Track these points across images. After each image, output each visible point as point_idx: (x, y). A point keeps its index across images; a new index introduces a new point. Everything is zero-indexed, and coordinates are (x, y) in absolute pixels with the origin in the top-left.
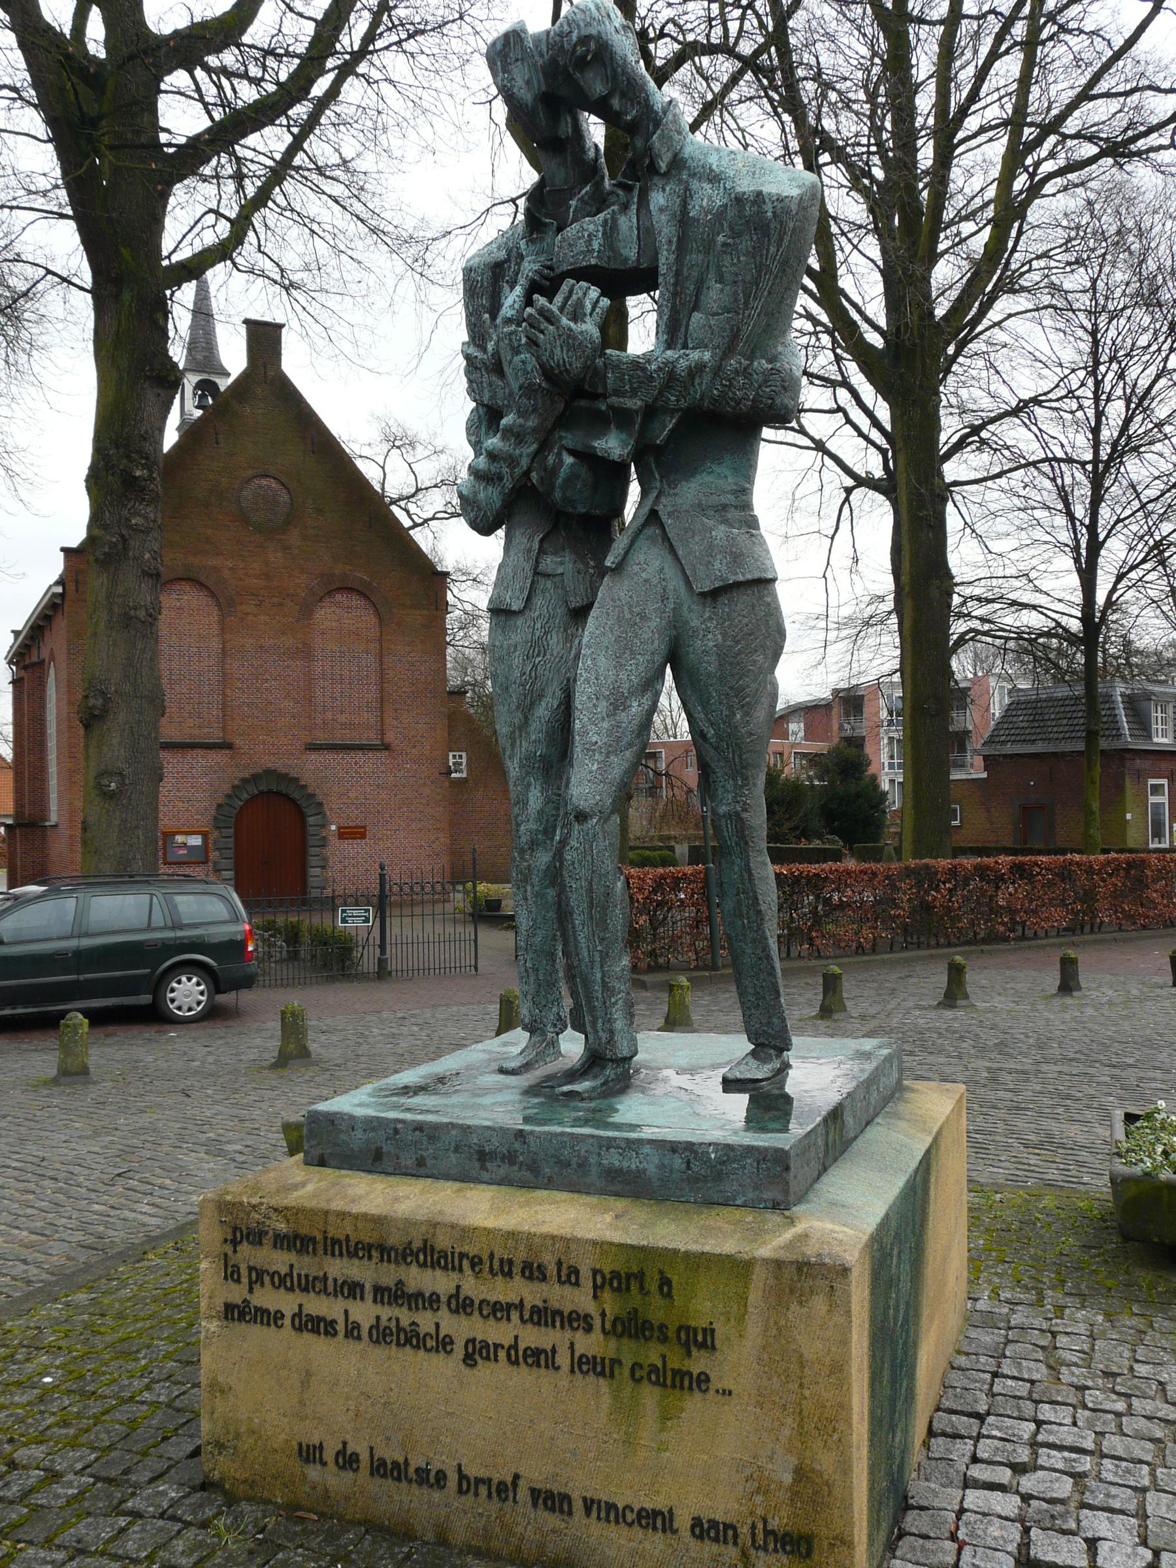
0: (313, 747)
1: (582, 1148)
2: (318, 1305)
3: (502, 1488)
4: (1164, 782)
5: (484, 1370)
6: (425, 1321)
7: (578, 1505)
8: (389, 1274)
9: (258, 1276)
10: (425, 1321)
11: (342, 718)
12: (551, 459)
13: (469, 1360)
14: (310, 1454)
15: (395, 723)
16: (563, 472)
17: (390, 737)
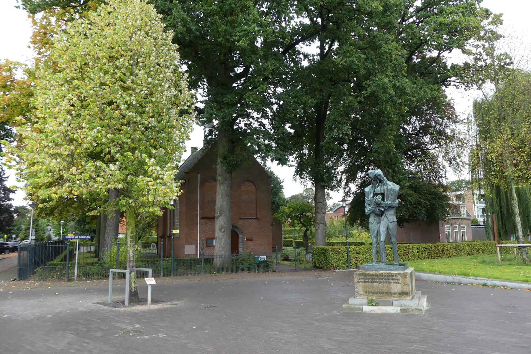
0: (240, 219)
8: (372, 277)
11: (247, 212)
17: (258, 216)
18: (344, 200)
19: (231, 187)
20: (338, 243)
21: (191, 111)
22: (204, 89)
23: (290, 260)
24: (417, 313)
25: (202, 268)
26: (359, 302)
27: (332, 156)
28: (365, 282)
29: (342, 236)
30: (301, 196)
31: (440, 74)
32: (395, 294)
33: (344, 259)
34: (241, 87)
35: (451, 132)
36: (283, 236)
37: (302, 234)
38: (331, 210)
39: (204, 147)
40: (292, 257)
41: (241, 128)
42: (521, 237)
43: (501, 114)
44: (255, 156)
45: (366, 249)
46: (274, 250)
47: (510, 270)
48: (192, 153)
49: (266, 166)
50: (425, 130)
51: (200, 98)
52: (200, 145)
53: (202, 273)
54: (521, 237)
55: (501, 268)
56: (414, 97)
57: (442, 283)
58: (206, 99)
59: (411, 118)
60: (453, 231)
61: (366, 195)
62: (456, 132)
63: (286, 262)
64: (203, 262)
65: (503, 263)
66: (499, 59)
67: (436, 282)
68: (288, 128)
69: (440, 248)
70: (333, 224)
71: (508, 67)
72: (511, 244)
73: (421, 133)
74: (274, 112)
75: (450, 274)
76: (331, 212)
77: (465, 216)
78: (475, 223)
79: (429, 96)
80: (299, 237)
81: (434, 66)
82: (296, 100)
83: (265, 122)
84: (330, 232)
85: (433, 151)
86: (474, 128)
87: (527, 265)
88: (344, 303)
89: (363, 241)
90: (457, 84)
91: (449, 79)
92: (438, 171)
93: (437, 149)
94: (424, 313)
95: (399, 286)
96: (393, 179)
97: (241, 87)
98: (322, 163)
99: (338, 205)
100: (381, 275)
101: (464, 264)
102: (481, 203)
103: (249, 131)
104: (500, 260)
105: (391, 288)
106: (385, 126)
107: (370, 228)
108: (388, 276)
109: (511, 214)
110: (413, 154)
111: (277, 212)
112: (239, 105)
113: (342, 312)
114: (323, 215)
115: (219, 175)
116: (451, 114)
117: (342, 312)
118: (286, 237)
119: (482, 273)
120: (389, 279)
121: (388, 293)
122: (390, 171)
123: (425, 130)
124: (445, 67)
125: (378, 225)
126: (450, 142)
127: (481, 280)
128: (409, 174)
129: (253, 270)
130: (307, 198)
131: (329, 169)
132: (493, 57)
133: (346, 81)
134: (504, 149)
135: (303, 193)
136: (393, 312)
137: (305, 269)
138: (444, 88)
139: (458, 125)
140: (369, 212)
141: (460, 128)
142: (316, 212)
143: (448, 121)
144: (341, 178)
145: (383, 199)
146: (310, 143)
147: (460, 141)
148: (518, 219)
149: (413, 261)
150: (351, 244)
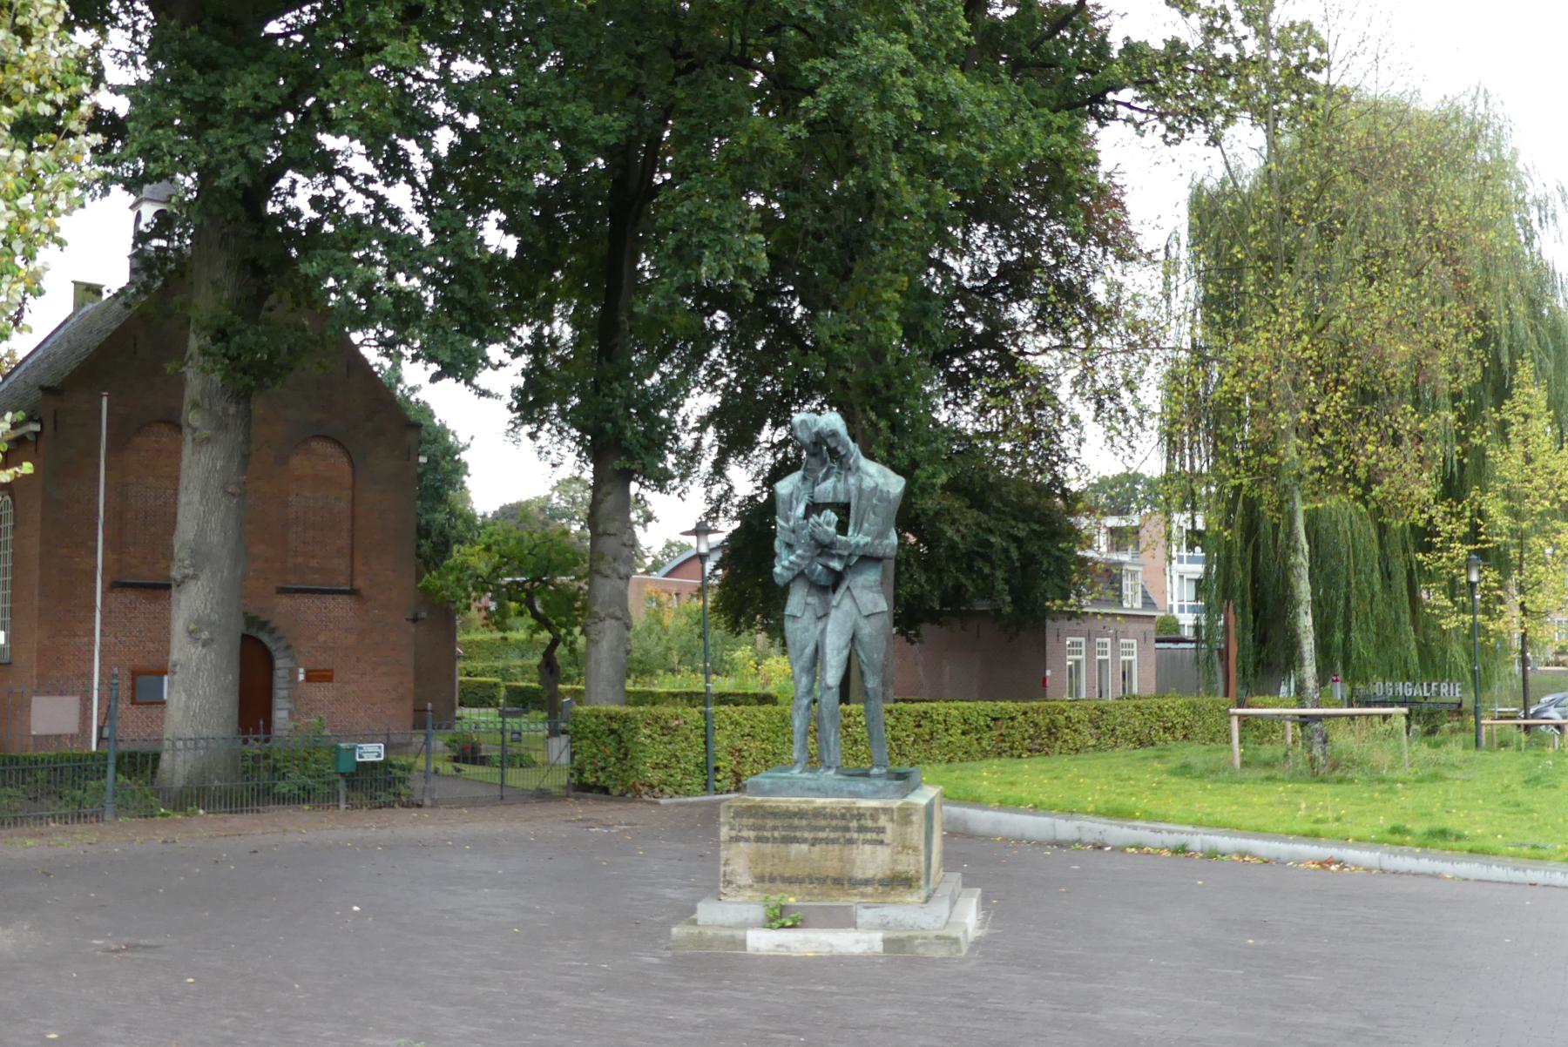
0: (282, 591)
8: (787, 822)
10: (798, 834)
11: (314, 563)
17: (359, 583)
18: (700, 530)
19: (246, 457)
20: (675, 695)
21: (73, 125)
22: (136, 33)
23: (483, 761)
24: (941, 952)
25: (108, 797)
26: (734, 916)
27: (662, 355)
28: (759, 839)
29: (694, 671)
30: (542, 510)
31: (1082, 71)
32: (866, 882)
33: (694, 755)
34: (298, 38)
35: (1108, 293)
36: (460, 665)
37: (537, 660)
38: (657, 566)
39: (131, 283)
40: (490, 749)
41: (296, 214)
42: (1311, 683)
43: (1277, 240)
44: (356, 337)
45: (776, 719)
46: (419, 723)
47: (1264, 800)
48: (78, 304)
49: (399, 380)
50: (1015, 279)
51: (116, 74)
52: (115, 275)
53: (108, 817)
54: (1311, 683)
55: (1237, 789)
56: (982, 148)
57: (1040, 843)
58: (145, 74)
59: (967, 231)
60: (1096, 659)
61: (780, 507)
62: (1126, 295)
63: (468, 769)
64: (111, 770)
65: (1247, 773)
66: (1284, 45)
67: (1019, 840)
68: (496, 237)
69: (1042, 720)
70: (659, 622)
71: (1311, 75)
72: (1278, 706)
73: (1003, 290)
74: (435, 160)
75: (1070, 812)
76: (655, 576)
77: (1138, 604)
78: (1168, 632)
79: (1037, 150)
80: (524, 671)
81: (1063, 38)
82: (537, 115)
83: (400, 195)
84: (647, 652)
85: (1040, 361)
86: (1187, 289)
87: (1323, 781)
88: (676, 921)
89: (771, 690)
90: (1139, 117)
91: (1110, 96)
92: (1052, 435)
93: (1056, 353)
94: (965, 950)
95: (883, 853)
96: (890, 454)
97: (298, 38)
98: (621, 375)
99: (683, 548)
100: (818, 813)
101: (1118, 778)
102: (1191, 560)
103: (328, 228)
104: (1237, 762)
105: (853, 862)
106: (873, 253)
107: (788, 635)
108: (843, 817)
109: (1286, 600)
110: (972, 368)
111: (437, 566)
112: (290, 118)
113: (669, 954)
114: (621, 584)
115: (195, 405)
116: (1112, 228)
117: (669, 954)
118: (469, 670)
119: (1176, 807)
120: (847, 829)
121: (843, 882)
122: (883, 424)
123: (1015, 279)
124: (1102, 48)
125: (820, 625)
126: (1101, 329)
127: (1170, 832)
128: (952, 440)
129: (331, 799)
130: (564, 514)
131: (649, 404)
132: (1264, 32)
133: (736, 61)
134: (1278, 368)
135: (548, 498)
136: (857, 949)
137: (542, 795)
138: (1092, 126)
139: (1132, 267)
140: (788, 575)
141: (1140, 280)
142: (593, 572)
143: (1100, 251)
144: (698, 442)
145: (842, 528)
146: (583, 294)
147: (1135, 330)
148: (1306, 621)
149: (944, 766)
150: (723, 699)
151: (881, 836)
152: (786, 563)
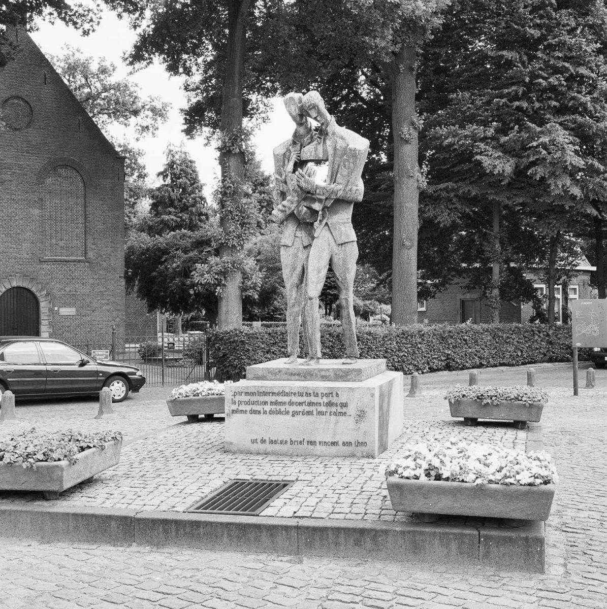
1: (316, 371)
2: (256, 408)
3: (301, 442)
4: (577, 287)
5: (297, 417)
6: (283, 408)
7: (318, 443)
8: (273, 399)
9: (240, 403)
10: (283, 408)
12: (300, 208)
13: (293, 415)
14: (254, 441)
15: (93, 247)
16: (303, 212)
151: (344, 410)
152: (280, 207)
